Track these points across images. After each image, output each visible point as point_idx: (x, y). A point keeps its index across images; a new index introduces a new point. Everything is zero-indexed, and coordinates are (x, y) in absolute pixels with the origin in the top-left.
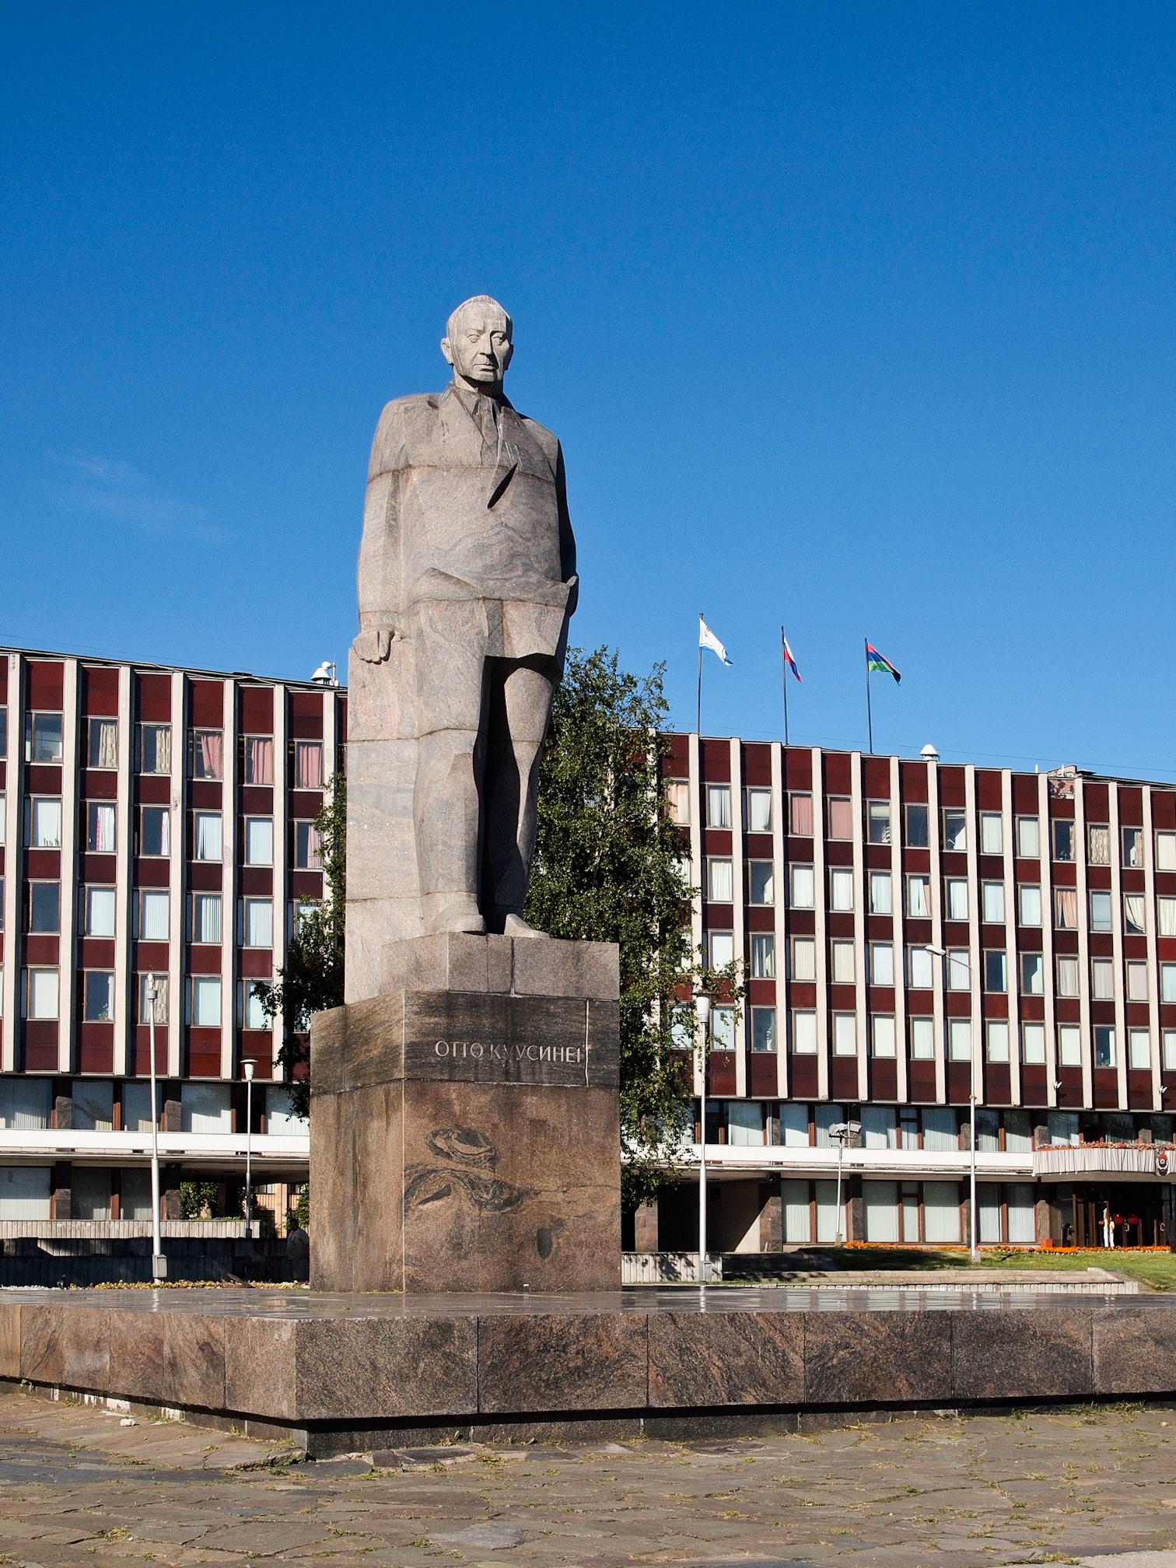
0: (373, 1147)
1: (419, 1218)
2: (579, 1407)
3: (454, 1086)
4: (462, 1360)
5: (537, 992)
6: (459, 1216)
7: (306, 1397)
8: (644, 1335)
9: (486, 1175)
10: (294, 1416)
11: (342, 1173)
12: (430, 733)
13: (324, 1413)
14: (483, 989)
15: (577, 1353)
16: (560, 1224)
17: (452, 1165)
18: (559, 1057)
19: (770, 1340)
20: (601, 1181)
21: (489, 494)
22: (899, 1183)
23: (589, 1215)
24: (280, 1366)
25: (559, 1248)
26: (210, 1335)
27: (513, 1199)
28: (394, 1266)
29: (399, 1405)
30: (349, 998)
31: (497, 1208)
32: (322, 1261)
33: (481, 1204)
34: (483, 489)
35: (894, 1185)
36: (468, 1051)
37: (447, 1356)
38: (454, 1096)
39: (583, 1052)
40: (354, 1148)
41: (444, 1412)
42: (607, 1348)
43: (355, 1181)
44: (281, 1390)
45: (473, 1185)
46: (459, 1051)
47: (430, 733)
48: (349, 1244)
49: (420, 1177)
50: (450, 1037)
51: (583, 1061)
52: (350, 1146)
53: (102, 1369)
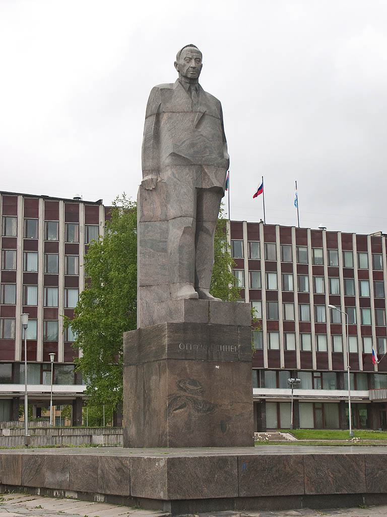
0: (153, 387)
1: (174, 416)
2: (278, 494)
3: (186, 362)
4: (232, 474)
5: (219, 323)
6: (190, 415)
7: (171, 490)
8: (302, 463)
9: (200, 398)
10: (166, 498)
11: (138, 398)
12: (174, 218)
13: (179, 497)
14: (198, 321)
15: (276, 471)
16: (230, 418)
17: (186, 394)
18: (228, 350)
19: (352, 466)
20: (245, 401)
21: (195, 122)
22: (314, 403)
23: (242, 415)
24: (159, 477)
25: (229, 429)
26: (122, 464)
27: (211, 408)
28: (163, 437)
29: (207, 493)
30: (139, 325)
31: (204, 412)
32: (129, 435)
33: (198, 411)
34: (193, 121)
35: (312, 405)
36: (192, 347)
37: (226, 472)
38: (187, 366)
39: (237, 347)
40: (144, 387)
41: (225, 496)
42: (288, 469)
43: (144, 401)
44: (159, 487)
45: (195, 402)
46: (189, 348)
47: (174, 218)
48: (142, 428)
49: (174, 399)
50: (185, 342)
51: (237, 351)
52: (142, 387)
53: (65, 480)
